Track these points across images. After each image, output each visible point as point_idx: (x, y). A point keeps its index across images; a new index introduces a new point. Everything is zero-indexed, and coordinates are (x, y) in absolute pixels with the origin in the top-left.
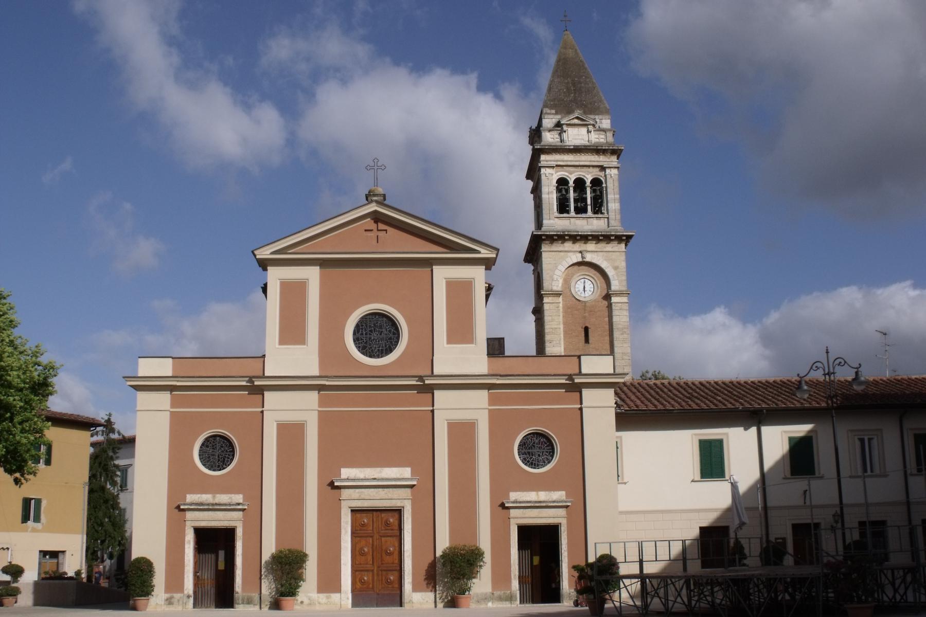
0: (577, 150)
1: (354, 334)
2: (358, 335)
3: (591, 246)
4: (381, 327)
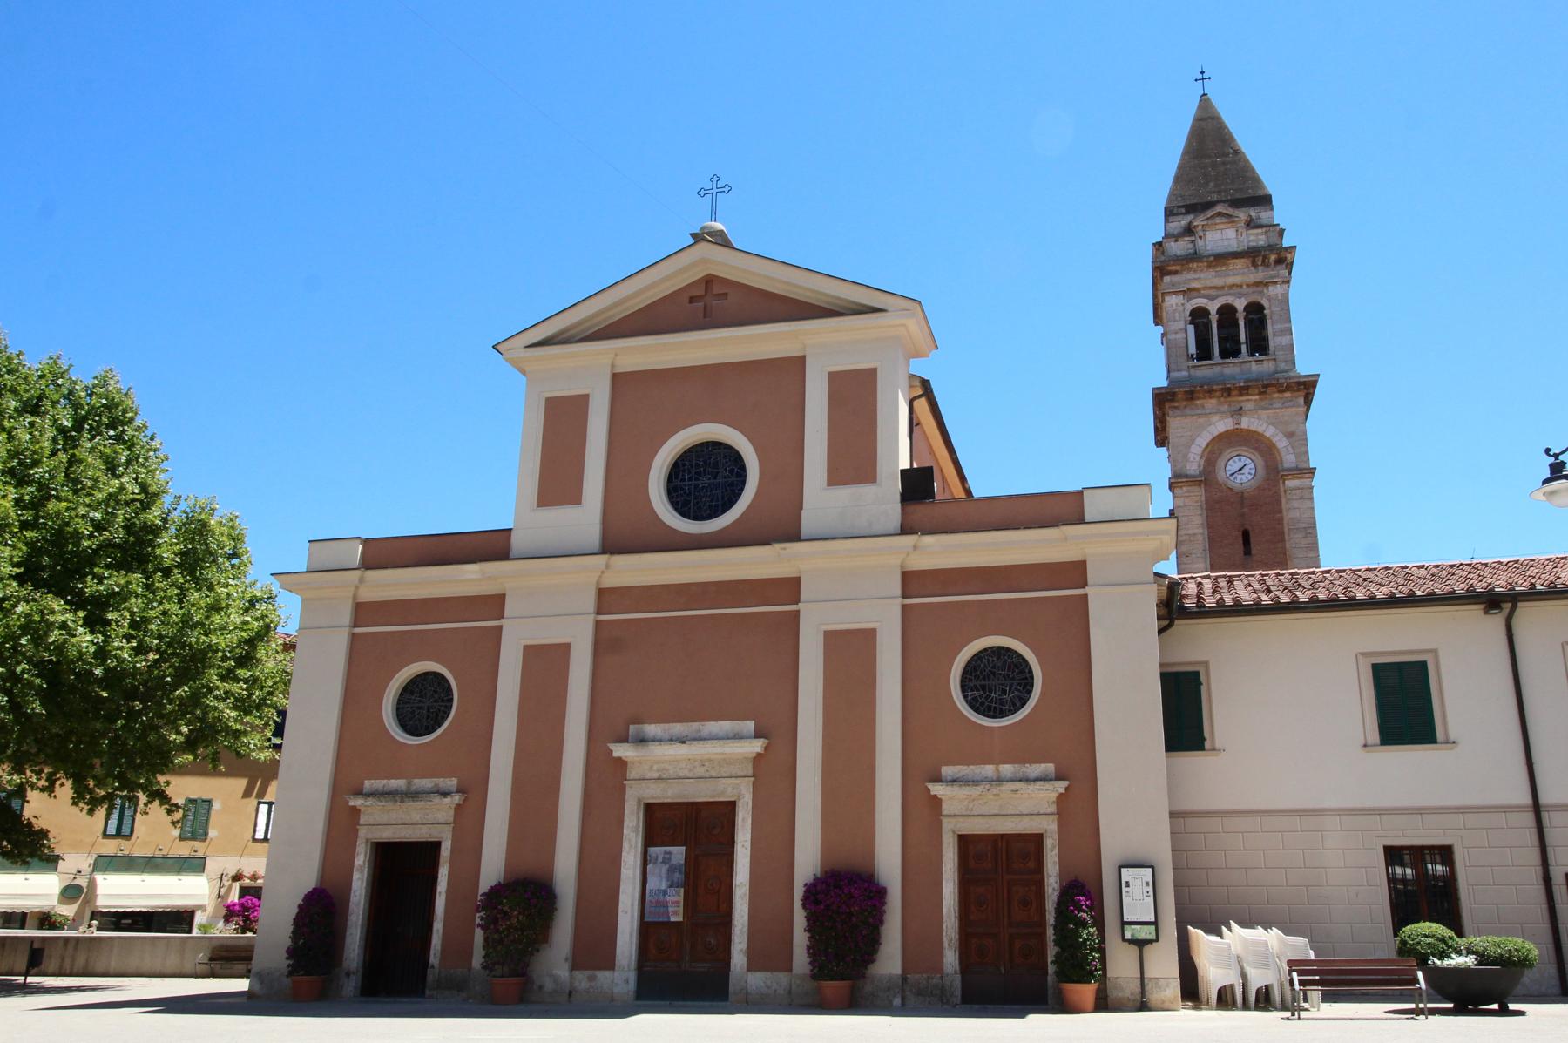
0: (1221, 258)
2: (677, 483)
3: (1249, 402)
4: (716, 465)
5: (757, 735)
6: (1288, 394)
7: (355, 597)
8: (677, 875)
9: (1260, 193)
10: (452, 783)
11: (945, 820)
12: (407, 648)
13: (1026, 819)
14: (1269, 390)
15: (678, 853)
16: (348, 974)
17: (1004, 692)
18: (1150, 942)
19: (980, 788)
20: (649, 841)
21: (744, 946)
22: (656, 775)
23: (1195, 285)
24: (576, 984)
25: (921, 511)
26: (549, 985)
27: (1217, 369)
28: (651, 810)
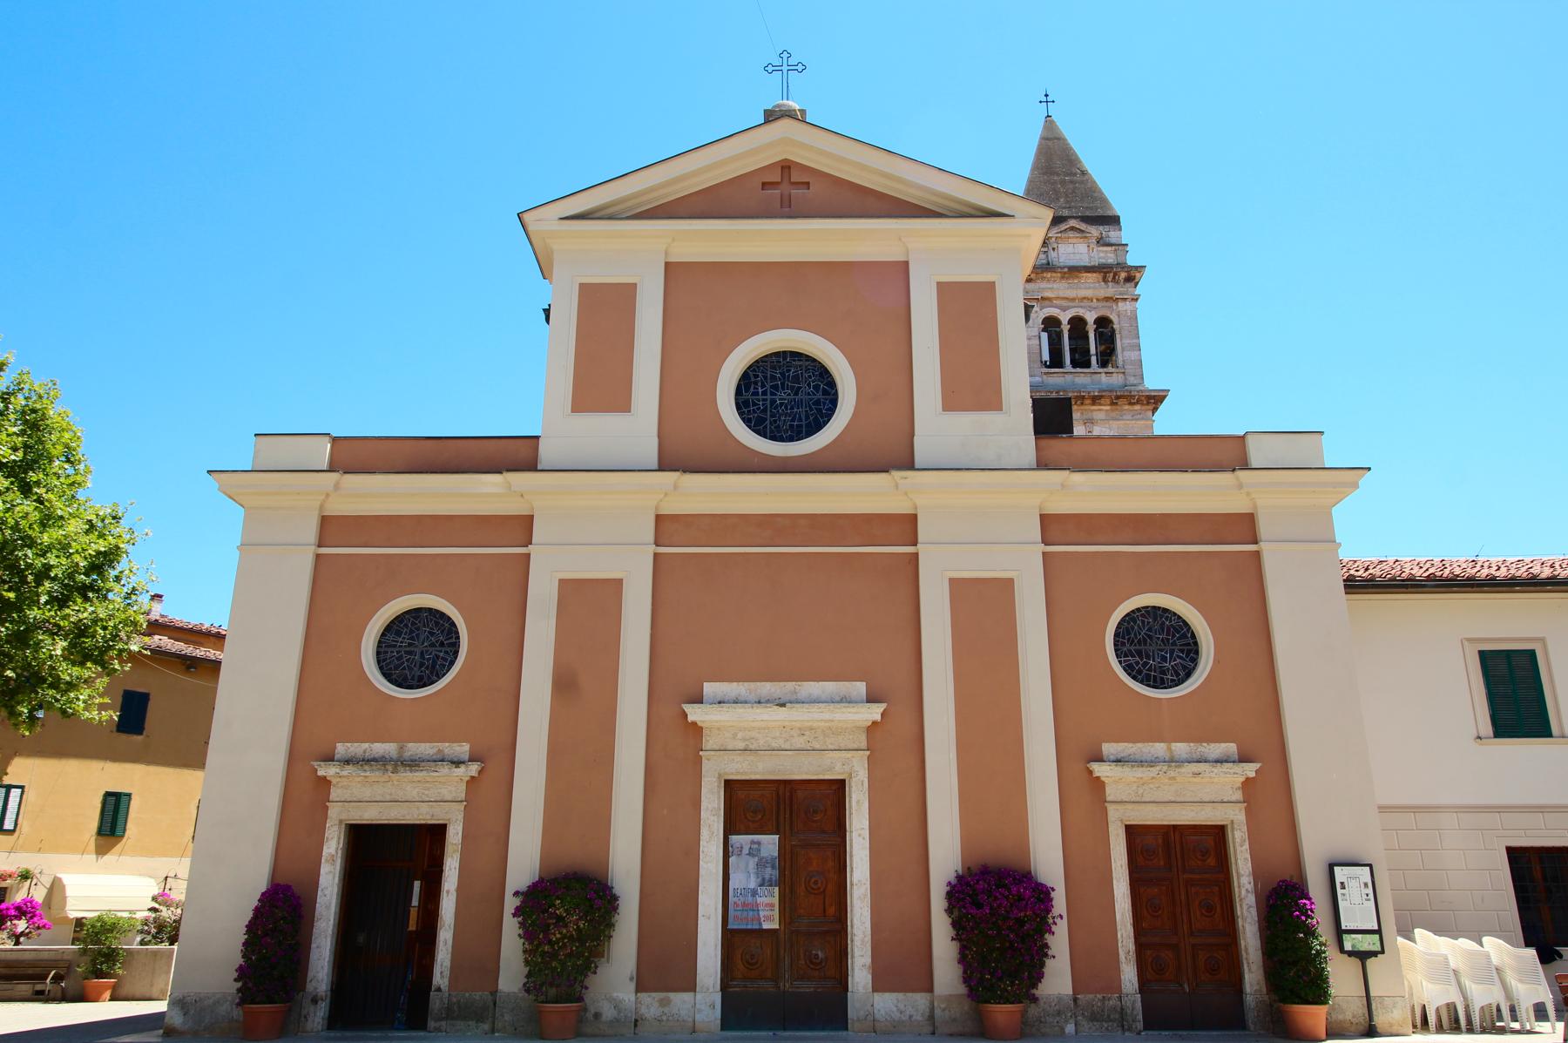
0: (1074, 271)
1: (738, 392)
2: (747, 396)
5: (871, 699)
6: (1137, 407)
7: (321, 507)
8: (769, 870)
9: (1110, 213)
10: (463, 749)
11: (1111, 808)
12: (396, 576)
13: (1208, 808)
14: (1120, 402)
15: (770, 844)
16: (315, 1001)
17: (1164, 659)
18: (1374, 954)
19: (1155, 770)
20: (730, 828)
21: (868, 960)
22: (741, 745)
23: (1047, 294)
24: (643, 1010)
25: (1057, 445)
26: (608, 1013)
27: (1069, 378)
28: (732, 788)
